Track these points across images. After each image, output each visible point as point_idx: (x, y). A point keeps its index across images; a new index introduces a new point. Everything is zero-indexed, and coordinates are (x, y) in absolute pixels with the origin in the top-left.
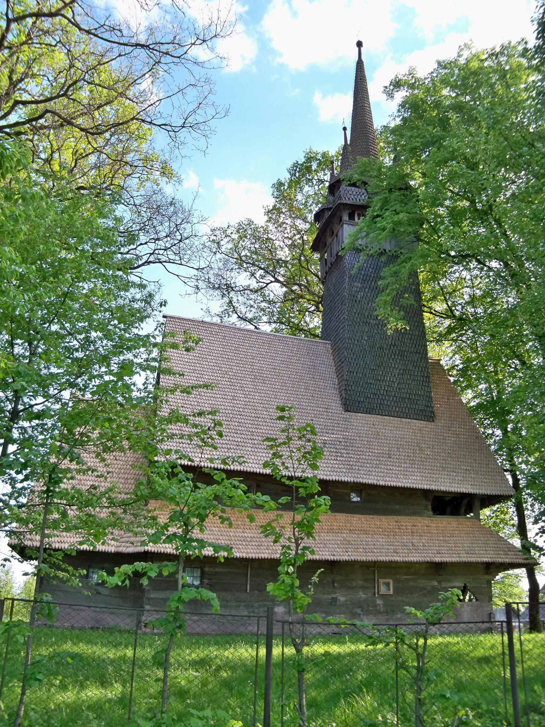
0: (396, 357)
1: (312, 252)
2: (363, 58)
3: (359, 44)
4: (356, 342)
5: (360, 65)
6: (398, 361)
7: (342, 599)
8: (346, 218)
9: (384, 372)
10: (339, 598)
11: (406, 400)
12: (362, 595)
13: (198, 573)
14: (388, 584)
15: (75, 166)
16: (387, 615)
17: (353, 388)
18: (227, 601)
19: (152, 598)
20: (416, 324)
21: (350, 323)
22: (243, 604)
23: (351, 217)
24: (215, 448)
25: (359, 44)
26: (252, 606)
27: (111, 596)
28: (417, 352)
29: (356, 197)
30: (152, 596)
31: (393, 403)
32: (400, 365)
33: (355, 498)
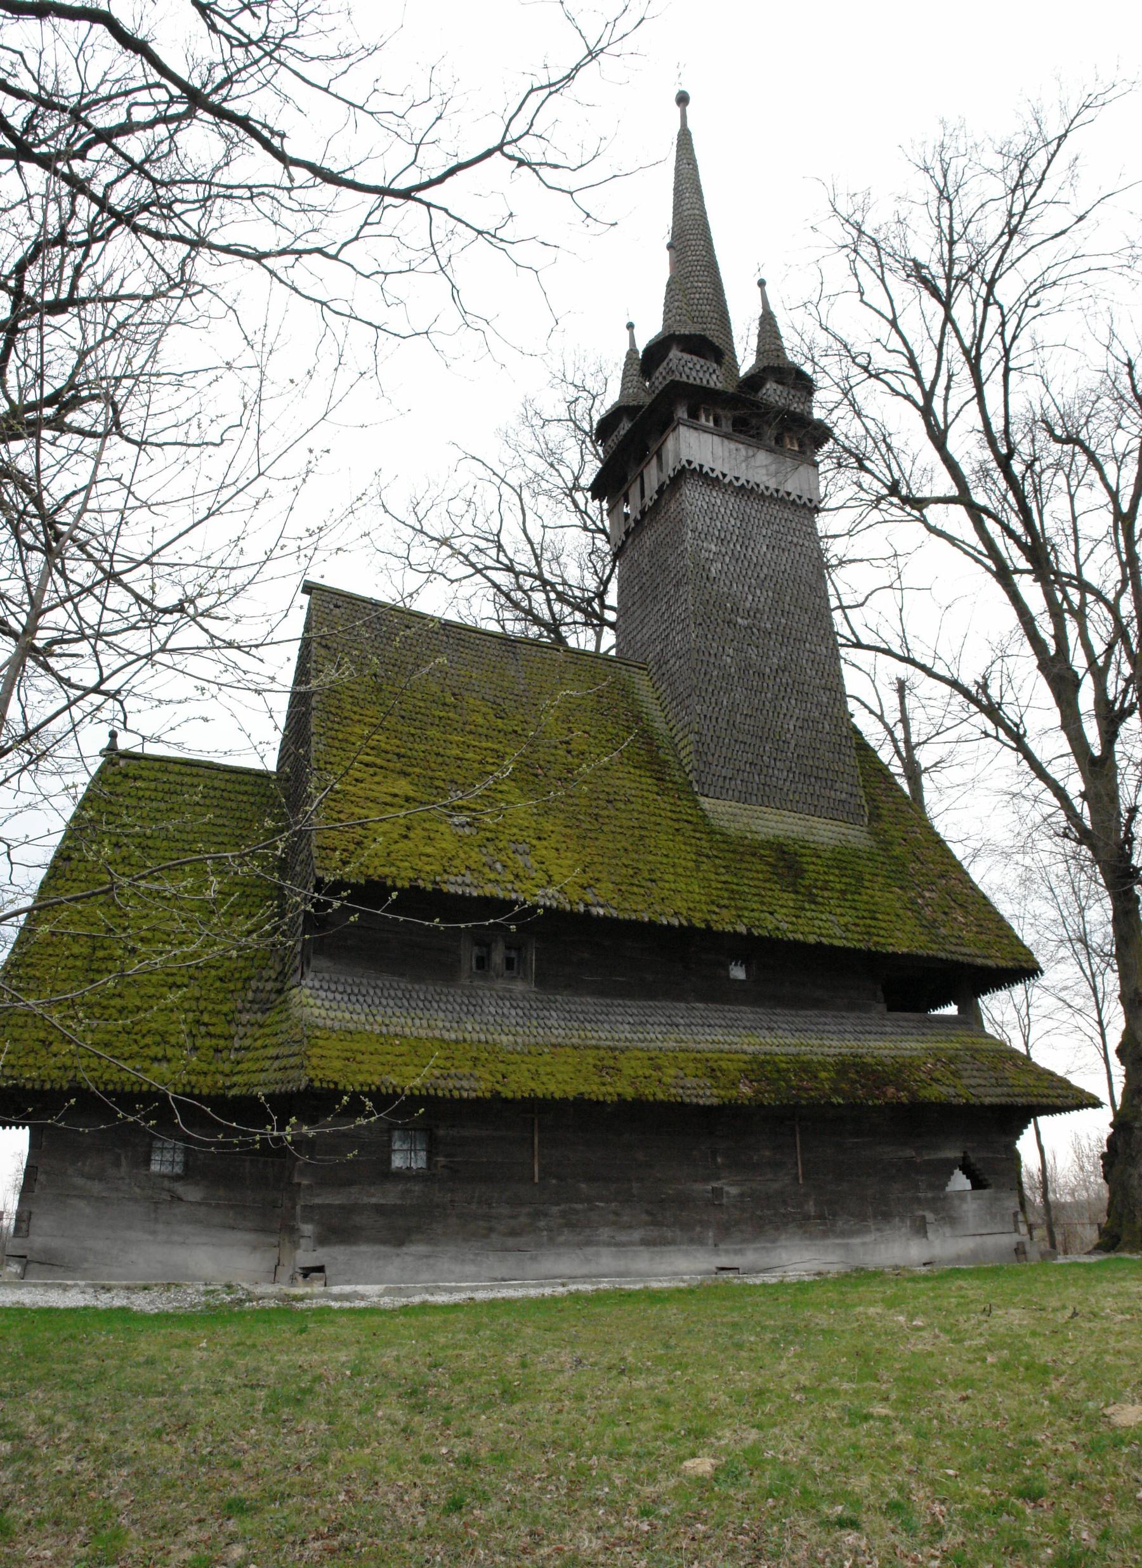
2: (690, 126)
3: (683, 99)
5: (685, 140)
7: (734, 1191)
8: (682, 413)
10: (726, 1188)
18: (490, 1205)
21: (700, 620)
23: (694, 415)
24: (169, 1061)
27: (209, 1205)
30: (318, 1201)
33: (738, 973)
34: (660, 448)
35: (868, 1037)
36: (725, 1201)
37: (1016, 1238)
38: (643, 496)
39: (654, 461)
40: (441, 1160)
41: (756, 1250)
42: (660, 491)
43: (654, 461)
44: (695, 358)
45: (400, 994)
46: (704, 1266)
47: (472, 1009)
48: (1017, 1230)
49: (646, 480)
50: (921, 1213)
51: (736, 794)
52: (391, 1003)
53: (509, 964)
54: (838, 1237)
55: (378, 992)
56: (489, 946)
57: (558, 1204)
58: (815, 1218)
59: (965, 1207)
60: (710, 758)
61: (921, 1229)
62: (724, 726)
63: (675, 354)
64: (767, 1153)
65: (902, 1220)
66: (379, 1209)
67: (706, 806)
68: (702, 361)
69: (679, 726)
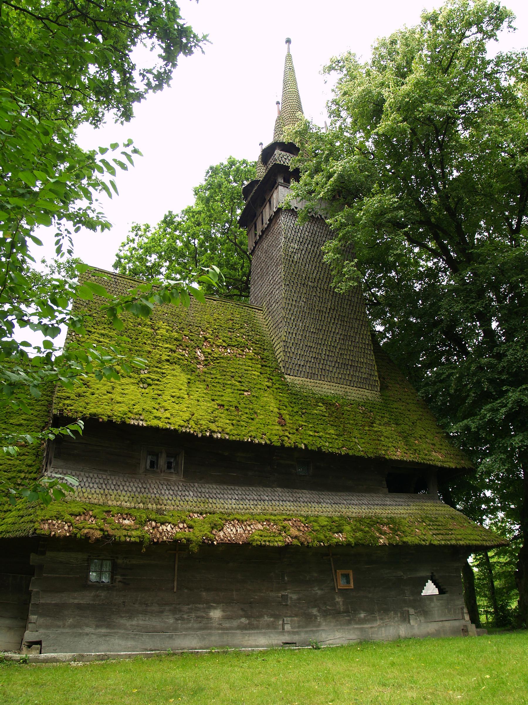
0: (336, 322)
3: (288, 41)
4: (294, 303)
5: (289, 58)
6: (338, 326)
7: (295, 597)
8: (281, 180)
10: (290, 595)
11: (349, 367)
12: (318, 591)
13: (107, 566)
16: (349, 616)
17: (293, 350)
18: (147, 605)
19: (43, 604)
21: (288, 283)
22: (167, 608)
23: (287, 181)
25: (288, 41)
26: (180, 611)
28: (356, 319)
30: (42, 601)
34: (270, 198)
35: (376, 507)
36: (289, 602)
37: (463, 622)
38: (263, 224)
39: (268, 204)
40: (119, 578)
41: (306, 632)
42: (270, 220)
43: (268, 204)
44: (288, 154)
45: (101, 481)
46: (275, 642)
47: (143, 490)
48: (463, 618)
49: (264, 215)
50: (406, 609)
51: (306, 374)
52: (96, 486)
53: (169, 466)
54: (357, 623)
55: (89, 480)
56: (157, 456)
57: (188, 605)
58: (344, 612)
59: (433, 605)
60: (291, 355)
61: (405, 618)
62: (300, 338)
63: (277, 152)
64: (315, 575)
65: (396, 613)
66: (79, 607)
67: (288, 380)
68: (292, 156)
69: (276, 339)
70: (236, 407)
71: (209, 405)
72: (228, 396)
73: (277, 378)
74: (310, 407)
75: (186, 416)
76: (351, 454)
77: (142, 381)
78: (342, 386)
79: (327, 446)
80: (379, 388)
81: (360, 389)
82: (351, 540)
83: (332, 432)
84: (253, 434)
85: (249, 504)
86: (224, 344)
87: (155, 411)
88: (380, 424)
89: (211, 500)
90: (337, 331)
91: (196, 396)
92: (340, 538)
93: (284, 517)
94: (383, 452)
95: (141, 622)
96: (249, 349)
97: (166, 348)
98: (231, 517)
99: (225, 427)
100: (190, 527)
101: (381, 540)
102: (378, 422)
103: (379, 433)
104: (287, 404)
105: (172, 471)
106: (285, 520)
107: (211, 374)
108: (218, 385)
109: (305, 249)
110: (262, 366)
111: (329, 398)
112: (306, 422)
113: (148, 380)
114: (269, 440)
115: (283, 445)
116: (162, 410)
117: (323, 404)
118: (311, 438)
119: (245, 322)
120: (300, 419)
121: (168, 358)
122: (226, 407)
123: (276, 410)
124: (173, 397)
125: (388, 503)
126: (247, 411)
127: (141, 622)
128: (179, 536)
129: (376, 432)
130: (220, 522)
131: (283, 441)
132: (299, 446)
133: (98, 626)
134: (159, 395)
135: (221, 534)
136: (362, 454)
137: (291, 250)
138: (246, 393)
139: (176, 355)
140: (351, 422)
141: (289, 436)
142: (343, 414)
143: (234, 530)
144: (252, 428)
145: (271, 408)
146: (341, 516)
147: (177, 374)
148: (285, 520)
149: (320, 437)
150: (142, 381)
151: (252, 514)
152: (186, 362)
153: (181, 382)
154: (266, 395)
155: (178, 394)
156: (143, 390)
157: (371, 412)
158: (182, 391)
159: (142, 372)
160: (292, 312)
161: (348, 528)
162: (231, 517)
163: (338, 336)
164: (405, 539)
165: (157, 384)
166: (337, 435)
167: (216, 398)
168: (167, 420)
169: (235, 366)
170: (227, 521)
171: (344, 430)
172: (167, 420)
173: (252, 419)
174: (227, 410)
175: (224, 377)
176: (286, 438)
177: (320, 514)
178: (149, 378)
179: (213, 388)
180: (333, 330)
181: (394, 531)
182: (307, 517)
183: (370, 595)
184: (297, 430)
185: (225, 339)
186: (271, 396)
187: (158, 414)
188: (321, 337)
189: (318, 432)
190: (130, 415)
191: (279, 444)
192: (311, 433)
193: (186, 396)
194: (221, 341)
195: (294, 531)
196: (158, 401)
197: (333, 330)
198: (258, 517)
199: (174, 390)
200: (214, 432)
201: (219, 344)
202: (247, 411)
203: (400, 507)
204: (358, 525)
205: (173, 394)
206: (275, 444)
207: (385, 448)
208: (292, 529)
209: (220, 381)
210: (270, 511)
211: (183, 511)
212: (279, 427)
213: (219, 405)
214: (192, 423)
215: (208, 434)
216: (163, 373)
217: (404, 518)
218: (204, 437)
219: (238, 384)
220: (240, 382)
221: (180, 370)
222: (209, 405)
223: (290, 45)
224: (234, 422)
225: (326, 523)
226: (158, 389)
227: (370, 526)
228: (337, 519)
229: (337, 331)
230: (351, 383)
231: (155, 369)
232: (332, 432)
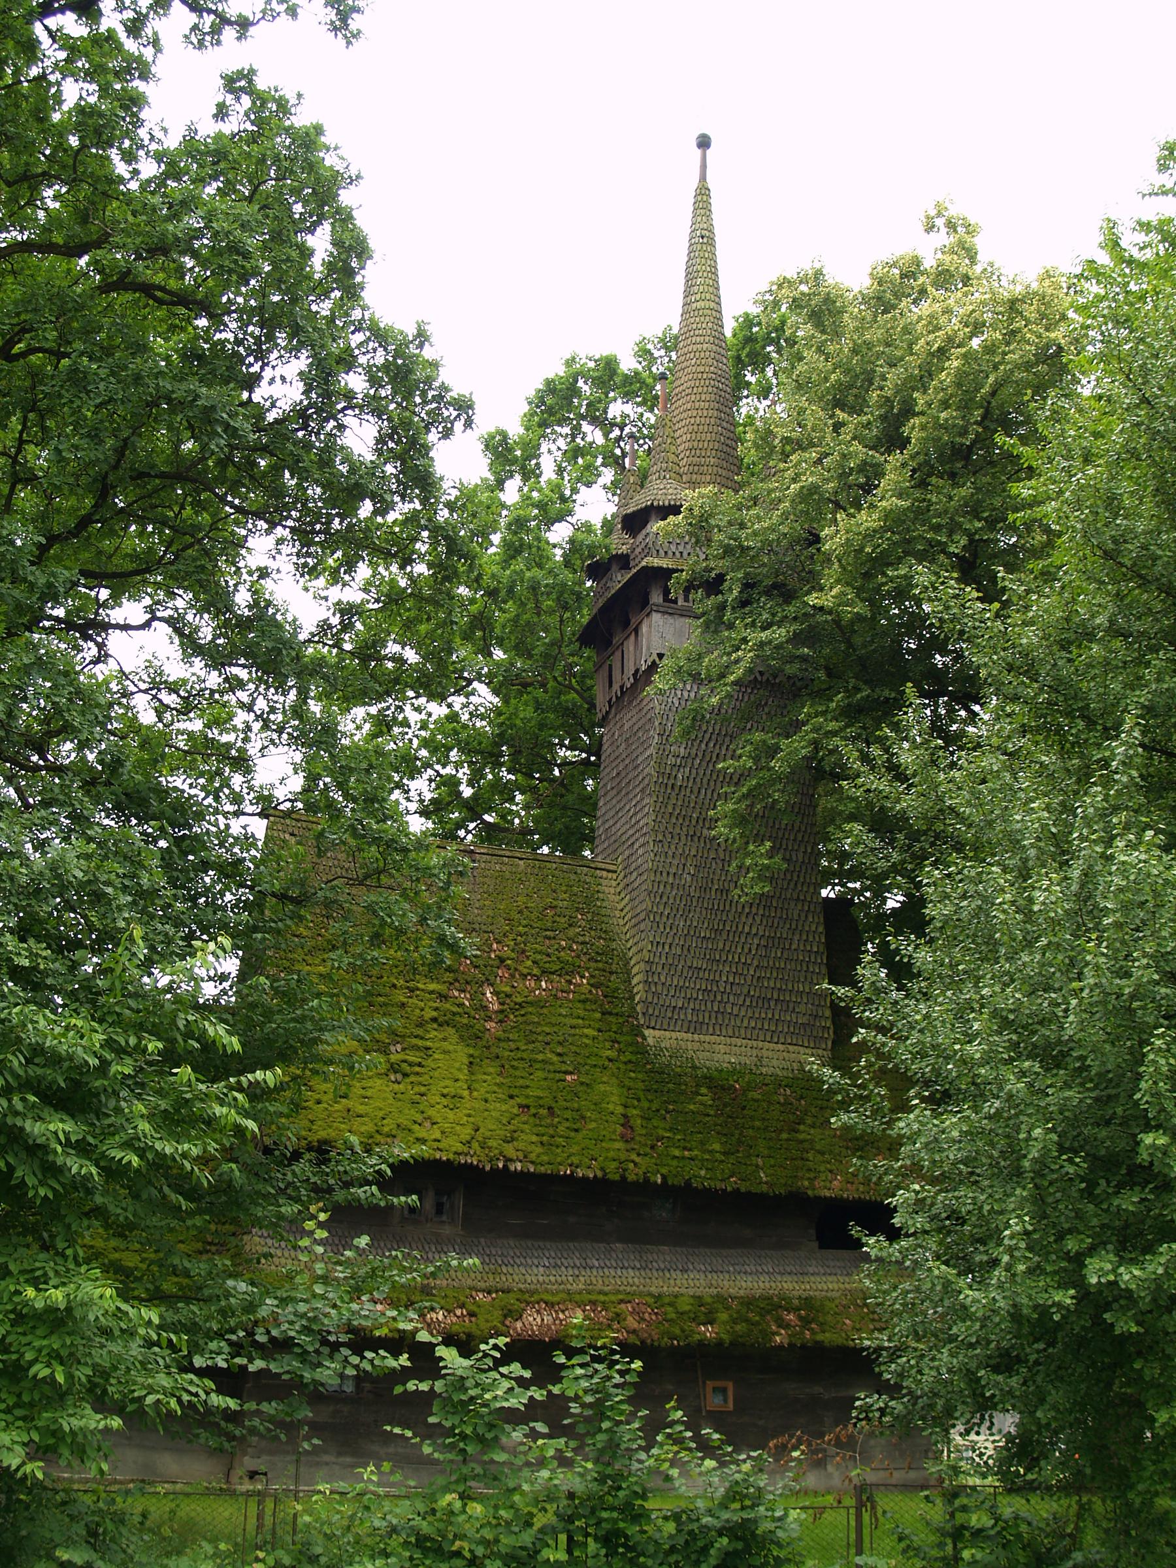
0: (754, 910)
1: (629, 1400)
3: (704, 143)
4: (671, 880)
5: (703, 194)
6: (758, 919)
9: (728, 944)
11: (772, 1003)
14: (724, 1391)
15: (40, 350)
17: (663, 979)
20: (799, 838)
21: (660, 837)
25: (704, 143)
29: (681, 548)
31: (743, 1009)
32: (761, 928)
51: (686, 1025)
60: (659, 988)
70: (550, 1108)
71: (504, 1108)
72: (537, 1089)
73: (629, 1038)
74: (682, 1098)
75: (466, 1133)
76: (743, 1190)
77: (394, 1068)
78: (755, 1043)
79: (701, 1177)
80: (830, 1044)
81: (791, 1048)
82: (724, 1336)
83: (717, 1146)
84: (575, 1160)
85: (566, 1275)
86: (536, 971)
87: (416, 1127)
88: (813, 1126)
89: (504, 1269)
90: (754, 931)
91: (483, 1090)
92: (708, 1332)
93: (621, 1297)
94: (806, 1183)
95: (400, 1450)
96: (582, 977)
97: (431, 992)
98: (535, 1298)
99: (530, 1148)
100: (472, 1314)
101: (778, 1339)
102: (809, 1121)
103: (806, 1145)
104: (641, 1094)
105: (444, 1218)
106: (621, 1301)
107: (509, 1040)
108: (521, 1065)
109: (700, 755)
110: (603, 1014)
111: (724, 1075)
112: (671, 1129)
113: (404, 1065)
114: (602, 1169)
115: (623, 1178)
116: (427, 1124)
117: (709, 1088)
118: (675, 1163)
119: (578, 909)
120: (662, 1124)
121: (435, 1014)
122: (533, 1111)
123: (620, 1110)
124: (444, 1096)
125: (811, 1270)
126: (568, 1114)
127: (400, 1450)
128: (455, 1328)
129: (802, 1142)
130: (518, 1306)
131: (625, 1170)
132: (652, 1179)
133: (340, 1454)
134: (422, 1095)
135: (519, 1325)
136: (765, 1188)
137: (671, 760)
138: (569, 1078)
139: (448, 1006)
140: (757, 1123)
141: (637, 1159)
142: (744, 1108)
143: (539, 1320)
144: (575, 1149)
145: (611, 1107)
146: (718, 1296)
147: (451, 1048)
148: (621, 1301)
149: (692, 1159)
150: (394, 1068)
151: (568, 1292)
152: (465, 1021)
153: (457, 1065)
154: (605, 1079)
155: (452, 1091)
156: (396, 1086)
157: (802, 1097)
158: (459, 1084)
159: (392, 1048)
160: (665, 899)
161: (723, 1316)
162: (535, 1298)
163: (756, 941)
164: (820, 1337)
165: (417, 1074)
166: (724, 1154)
167: (515, 1092)
168: (436, 1145)
169: (553, 1020)
170: (528, 1303)
171: (740, 1142)
172: (436, 1145)
173: (576, 1130)
174: (534, 1115)
175: (531, 1046)
176: (631, 1165)
177: (683, 1290)
178: (405, 1061)
179: (512, 1071)
180: (747, 929)
181: (806, 1322)
182: (658, 1297)
183: (761, 1423)
184: (652, 1147)
185: (539, 957)
186: (614, 1080)
187: (421, 1133)
188: (721, 946)
189: (690, 1150)
190: (379, 1138)
191: (617, 1177)
192: (677, 1153)
193: (466, 1093)
194: (529, 963)
195: (631, 1322)
196: (421, 1107)
197: (747, 929)
198: (577, 1298)
199: (447, 1082)
200: (511, 1160)
201: (525, 971)
202: (568, 1114)
203: (830, 1278)
204: (744, 1310)
205: (445, 1091)
206: (610, 1176)
207: (812, 1175)
208: (630, 1318)
209: (525, 1055)
210: (599, 1287)
211: (461, 1288)
212: (619, 1145)
213: (520, 1106)
214: (475, 1145)
215: (501, 1165)
216: (428, 1049)
217: (832, 1300)
218: (495, 1170)
219: (555, 1059)
220: (560, 1055)
221: (455, 1038)
222: (504, 1108)
223: (708, 152)
224: (545, 1138)
225: (687, 1308)
226: (420, 1084)
227: (763, 1313)
228: (709, 1300)
229: (754, 931)
230: (773, 1037)
231: (415, 1041)
232: (717, 1146)
